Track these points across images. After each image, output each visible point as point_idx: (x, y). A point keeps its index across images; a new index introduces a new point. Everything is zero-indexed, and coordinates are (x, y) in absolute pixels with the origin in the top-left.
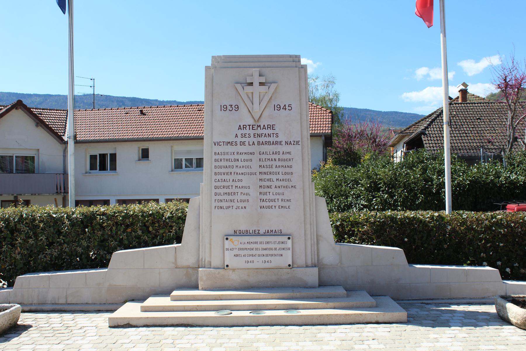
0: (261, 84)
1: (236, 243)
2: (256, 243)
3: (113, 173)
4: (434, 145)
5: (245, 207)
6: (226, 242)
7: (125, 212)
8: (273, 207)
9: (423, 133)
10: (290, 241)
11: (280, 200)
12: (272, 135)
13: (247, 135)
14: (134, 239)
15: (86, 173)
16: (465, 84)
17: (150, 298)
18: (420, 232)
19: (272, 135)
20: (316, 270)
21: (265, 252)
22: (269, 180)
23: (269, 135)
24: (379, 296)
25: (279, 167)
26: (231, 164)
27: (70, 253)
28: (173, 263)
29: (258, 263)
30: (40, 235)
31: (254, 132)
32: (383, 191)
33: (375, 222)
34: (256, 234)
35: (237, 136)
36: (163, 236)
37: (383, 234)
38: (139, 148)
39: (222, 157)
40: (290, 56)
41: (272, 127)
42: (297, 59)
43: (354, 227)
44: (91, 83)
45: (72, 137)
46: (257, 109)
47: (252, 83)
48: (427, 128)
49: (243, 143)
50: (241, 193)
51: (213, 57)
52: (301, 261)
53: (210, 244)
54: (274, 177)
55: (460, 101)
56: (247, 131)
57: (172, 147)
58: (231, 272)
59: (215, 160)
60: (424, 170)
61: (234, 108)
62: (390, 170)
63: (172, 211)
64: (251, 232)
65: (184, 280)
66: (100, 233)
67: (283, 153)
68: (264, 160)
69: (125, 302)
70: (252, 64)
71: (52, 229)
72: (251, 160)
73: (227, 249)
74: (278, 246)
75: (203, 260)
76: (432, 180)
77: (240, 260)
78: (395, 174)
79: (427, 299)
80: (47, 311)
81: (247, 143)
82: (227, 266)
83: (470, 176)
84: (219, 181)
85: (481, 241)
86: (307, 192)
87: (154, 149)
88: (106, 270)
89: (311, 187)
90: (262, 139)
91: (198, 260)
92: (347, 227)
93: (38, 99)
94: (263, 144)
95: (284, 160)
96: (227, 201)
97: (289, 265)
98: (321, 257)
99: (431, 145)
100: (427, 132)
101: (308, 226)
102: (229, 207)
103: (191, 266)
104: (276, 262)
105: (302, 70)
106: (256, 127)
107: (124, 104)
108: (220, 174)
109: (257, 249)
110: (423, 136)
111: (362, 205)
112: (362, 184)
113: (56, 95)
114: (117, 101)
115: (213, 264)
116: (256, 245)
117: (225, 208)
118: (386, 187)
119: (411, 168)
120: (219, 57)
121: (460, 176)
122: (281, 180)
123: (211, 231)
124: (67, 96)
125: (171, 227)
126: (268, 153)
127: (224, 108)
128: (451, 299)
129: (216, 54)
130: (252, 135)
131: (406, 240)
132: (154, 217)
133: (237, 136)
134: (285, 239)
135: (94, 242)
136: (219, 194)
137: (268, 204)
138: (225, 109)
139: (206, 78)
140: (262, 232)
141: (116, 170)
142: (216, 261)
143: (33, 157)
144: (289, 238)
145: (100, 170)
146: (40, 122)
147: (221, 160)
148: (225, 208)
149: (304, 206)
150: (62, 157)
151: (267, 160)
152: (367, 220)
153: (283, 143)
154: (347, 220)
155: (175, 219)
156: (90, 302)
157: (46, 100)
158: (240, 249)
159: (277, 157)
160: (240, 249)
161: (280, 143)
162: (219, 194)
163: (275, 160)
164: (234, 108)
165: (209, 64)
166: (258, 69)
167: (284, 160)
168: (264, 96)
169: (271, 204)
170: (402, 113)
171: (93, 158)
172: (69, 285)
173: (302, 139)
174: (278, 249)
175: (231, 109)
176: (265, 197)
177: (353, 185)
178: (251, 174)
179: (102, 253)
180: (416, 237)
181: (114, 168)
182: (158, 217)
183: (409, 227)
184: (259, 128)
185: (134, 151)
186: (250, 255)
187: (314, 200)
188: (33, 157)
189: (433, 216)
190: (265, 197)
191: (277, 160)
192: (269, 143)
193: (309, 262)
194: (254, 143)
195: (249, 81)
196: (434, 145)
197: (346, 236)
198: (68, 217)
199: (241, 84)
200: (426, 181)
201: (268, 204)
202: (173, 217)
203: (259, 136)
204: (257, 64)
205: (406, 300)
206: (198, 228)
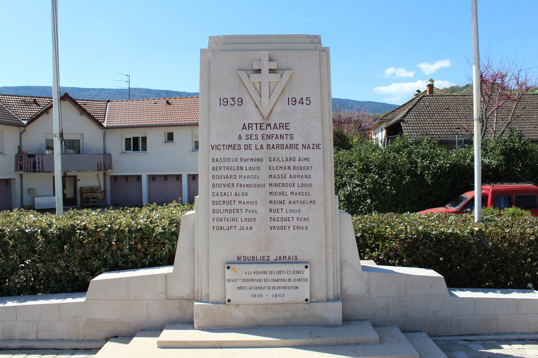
0: (272, 71)
1: (240, 272)
2: (265, 272)
3: (144, 153)
4: (411, 130)
5: (251, 228)
6: (228, 271)
7: (109, 226)
9: (402, 120)
10: (308, 270)
11: (295, 219)
12: (285, 136)
13: (254, 137)
14: (120, 258)
15: (122, 153)
16: (431, 80)
17: (134, 338)
18: (458, 249)
19: (285, 136)
21: (276, 284)
22: (282, 194)
23: (282, 137)
24: (414, 331)
25: (295, 176)
26: (233, 173)
27: (48, 273)
28: (163, 294)
29: (268, 297)
30: (11, 254)
32: (373, 172)
33: (406, 239)
36: (155, 255)
37: (415, 252)
38: (165, 132)
39: (222, 164)
40: (308, 37)
41: (285, 126)
42: (316, 40)
43: (378, 241)
44: (127, 79)
45: (58, 135)
46: (266, 104)
47: (260, 70)
48: (405, 116)
49: (248, 147)
50: (246, 210)
52: (321, 294)
53: (208, 273)
54: (288, 190)
55: (428, 93)
56: (253, 131)
57: (192, 131)
58: (233, 308)
59: (213, 168)
60: (410, 153)
61: (237, 102)
63: (165, 226)
64: (259, 258)
65: (176, 314)
66: (80, 251)
67: (300, 160)
68: (275, 168)
69: (107, 340)
70: (260, 46)
71: (25, 246)
73: (229, 281)
74: (293, 277)
75: (200, 292)
76: (416, 163)
77: (245, 295)
78: (385, 158)
79: (470, 335)
80: (14, 349)
81: (253, 147)
82: (229, 301)
83: (450, 160)
84: (218, 194)
85: (525, 258)
86: (329, 208)
87: (178, 133)
88: (82, 300)
89: (334, 201)
92: (370, 240)
93: (94, 92)
94: (273, 147)
95: (301, 168)
96: (228, 220)
97: (307, 300)
98: (344, 287)
99: (409, 131)
100: (405, 120)
101: (330, 251)
102: (231, 227)
104: (290, 296)
105: (323, 54)
106: (264, 126)
107: (160, 96)
108: (219, 186)
109: (266, 280)
111: (355, 184)
112: (355, 166)
114: (155, 93)
115: (211, 298)
116: (265, 275)
117: (225, 228)
118: (376, 169)
119: (398, 152)
120: (219, 37)
121: (440, 160)
124: (51, 88)
125: (164, 244)
126: (281, 160)
127: (224, 102)
128: (498, 334)
130: (260, 137)
131: (441, 259)
132: (143, 233)
134: (301, 267)
135: (74, 261)
136: (219, 211)
137: (280, 224)
138: (225, 104)
140: (272, 259)
141: (146, 150)
144: (306, 267)
146: (83, 112)
147: (220, 168)
148: (225, 228)
149: (326, 225)
150: (102, 140)
151: (278, 168)
152: (396, 236)
153: (300, 147)
154: (370, 232)
155: (167, 235)
156: (65, 338)
157: (100, 93)
158: (245, 280)
159: (291, 164)
160: (245, 280)
161: (296, 146)
162: (219, 211)
164: (237, 102)
165: (206, 47)
166: (267, 52)
167: (301, 168)
168: (275, 87)
169: (284, 223)
170: (375, 103)
171: (128, 140)
173: (323, 141)
174: (292, 280)
175: (233, 103)
176: (276, 215)
177: (347, 166)
178: (259, 186)
179: (83, 274)
180: (453, 256)
181: (144, 149)
182: (147, 233)
183: (446, 245)
184: (269, 128)
186: (257, 288)
187: (338, 218)
189: (473, 230)
190: (276, 215)
191: (292, 168)
192: (281, 147)
193: (331, 295)
194: (262, 147)
195: (256, 67)
196: (411, 130)
197: (367, 250)
198: (44, 233)
199: (246, 71)
200: (411, 163)
201: (280, 224)
202: (165, 232)
203: (269, 137)
204: (266, 46)
205: (445, 336)
206: (193, 251)
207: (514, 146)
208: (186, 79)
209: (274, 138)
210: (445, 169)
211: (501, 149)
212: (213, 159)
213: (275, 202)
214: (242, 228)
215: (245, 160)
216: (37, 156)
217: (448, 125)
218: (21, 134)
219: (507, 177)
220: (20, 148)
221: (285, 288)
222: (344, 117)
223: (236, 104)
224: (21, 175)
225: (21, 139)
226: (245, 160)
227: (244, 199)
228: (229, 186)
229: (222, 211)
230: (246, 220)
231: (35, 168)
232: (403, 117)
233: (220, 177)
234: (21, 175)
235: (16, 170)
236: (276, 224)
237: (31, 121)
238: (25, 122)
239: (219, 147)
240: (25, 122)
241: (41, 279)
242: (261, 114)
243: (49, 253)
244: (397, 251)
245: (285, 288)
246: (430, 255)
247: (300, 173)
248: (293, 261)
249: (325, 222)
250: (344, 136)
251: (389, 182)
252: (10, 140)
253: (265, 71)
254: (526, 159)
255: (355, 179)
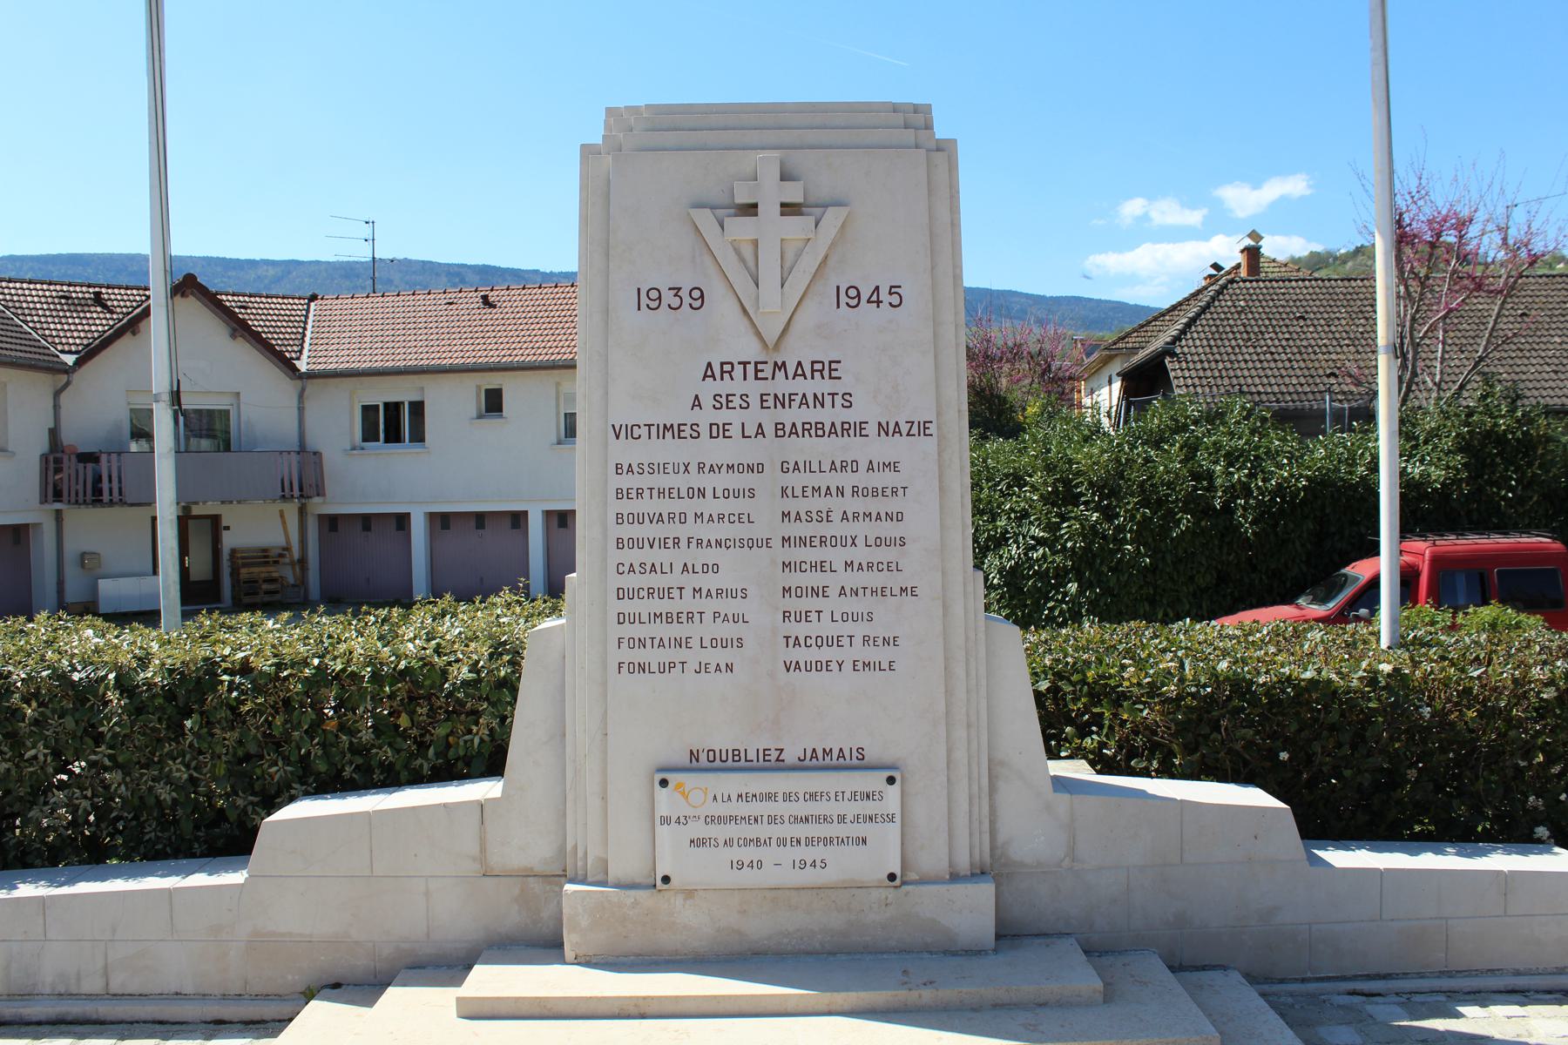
0: (788, 209)
1: (696, 797)
2: (771, 797)
3: (416, 448)
4: (1197, 381)
5: (729, 667)
6: (662, 794)
7: (316, 661)
8: (834, 666)
9: (1168, 352)
11: (858, 640)
12: (828, 399)
13: (737, 401)
17: (390, 989)
18: (1332, 728)
19: (828, 399)
20: (985, 893)
21: (802, 831)
22: (820, 566)
23: (819, 401)
24: (1204, 968)
25: (856, 516)
26: (676, 506)
27: (136, 801)
28: (474, 859)
29: (779, 868)
30: (28, 744)
31: (762, 387)
32: (1086, 503)
33: (1180, 697)
34: (771, 762)
35: (697, 402)
36: (448, 746)
37: (1206, 737)
38: (479, 387)
39: (645, 481)
40: (895, 108)
41: (828, 369)
42: (919, 119)
43: (1099, 703)
44: (366, 231)
45: (166, 397)
46: (772, 305)
47: (755, 206)
48: (1177, 339)
49: (720, 431)
50: (716, 615)
51: (610, 112)
52: (933, 859)
53: (604, 799)
54: (837, 556)
55: (1243, 273)
56: (735, 386)
59: (619, 491)
60: (1191, 449)
61: (687, 300)
62: (1103, 452)
63: (477, 662)
64: (752, 755)
65: (512, 918)
67: (870, 468)
68: (798, 492)
70: (754, 137)
71: (69, 722)
72: (752, 493)
73: (666, 820)
75: (580, 854)
76: (1210, 476)
77: (712, 862)
78: (1118, 460)
79: (1369, 977)
80: (39, 1023)
81: (735, 431)
82: (666, 879)
83: (1309, 468)
84: (632, 569)
85: (1528, 754)
86: (958, 610)
87: (514, 391)
89: (970, 588)
90: (794, 415)
91: (562, 849)
92: (1075, 700)
93: (271, 272)
96: (661, 644)
97: (892, 877)
99: (1189, 382)
100: (1178, 350)
101: (960, 733)
102: (672, 665)
103: (539, 868)
104: (844, 864)
105: (939, 158)
107: (463, 281)
109: (772, 820)
110: (1167, 360)
111: (1033, 538)
112: (1032, 486)
113: (310, 262)
115: (615, 872)
116: (771, 804)
117: (654, 668)
118: (1094, 494)
120: (634, 110)
121: (1280, 467)
122: (860, 567)
123: (605, 752)
124: (145, 258)
125: (475, 714)
126: (815, 467)
127: (650, 299)
129: (620, 103)
130: (754, 401)
131: (1284, 756)
132: (415, 683)
133: (697, 402)
134: (876, 781)
135: (214, 766)
136: (635, 619)
137: (813, 654)
138: (654, 304)
139: (584, 187)
140: (790, 757)
142: (625, 864)
143: (227, 412)
144: (891, 780)
145: (387, 441)
146: (240, 328)
147: (640, 493)
148: (654, 668)
150: (296, 411)
153: (871, 429)
155: (485, 689)
156: (189, 989)
157: (289, 272)
158: (711, 820)
159: (846, 480)
160: (711, 820)
161: (859, 429)
162: (635, 619)
163: (841, 491)
164: (687, 300)
165: (597, 139)
166: (776, 154)
168: (798, 255)
169: (826, 654)
170: (1090, 300)
171: (370, 411)
172: (114, 931)
173: (939, 414)
174: (849, 818)
175: (676, 302)
176: (801, 630)
177: (1009, 487)
178: (751, 544)
179: (240, 802)
181: (418, 436)
184: (780, 375)
185: (466, 394)
186: (748, 842)
187: (982, 636)
188: (227, 412)
189: (1376, 672)
190: (801, 630)
191: (848, 492)
192: (816, 430)
193: (963, 863)
194: (760, 431)
195: (742, 198)
196: (1197, 381)
197: (1068, 729)
198: (124, 685)
199: (713, 208)
200: (1197, 477)
201: (813, 654)
202: (479, 681)
203: (781, 401)
204: (771, 137)
207: (1496, 425)
208: (539, 232)
209: (795, 404)
210: (1295, 495)
211: (1458, 435)
212: (618, 467)
213: (800, 592)
214: (703, 668)
215: (712, 469)
216: (104, 458)
217: (1302, 364)
218: (57, 394)
219: (1475, 516)
220: (54, 433)
221: (828, 841)
222: (1000, 343)
223: (686, 306)
224: (58, 513)
225: (56, 407)
226: (712, 469)
227: (709, 582)
228: (664, 543)
229: (645, 618)
230: (715, 643)
231: (98, 491)
232: (1173, 342)
233: (638, 519)
234: (58, 513)
235: (44, 500)
236: (801, 655)
237: (88, 355)
238: (70, 360)
239: (636, 432)
240: (70, 360)
241: (118, 818)
242: (758, 334)
243: (139, 740)
244: (1155, 733)
245: (828, 841)
246: (1250, 744)
247: (874, 505)
248: (858, 763)
249: (946, 649)
250: (999, 397)
251: (1131, 531)
252: (26, 410)
253: (770, 209)
254: (1530, 465)
255: (1031, 523)
